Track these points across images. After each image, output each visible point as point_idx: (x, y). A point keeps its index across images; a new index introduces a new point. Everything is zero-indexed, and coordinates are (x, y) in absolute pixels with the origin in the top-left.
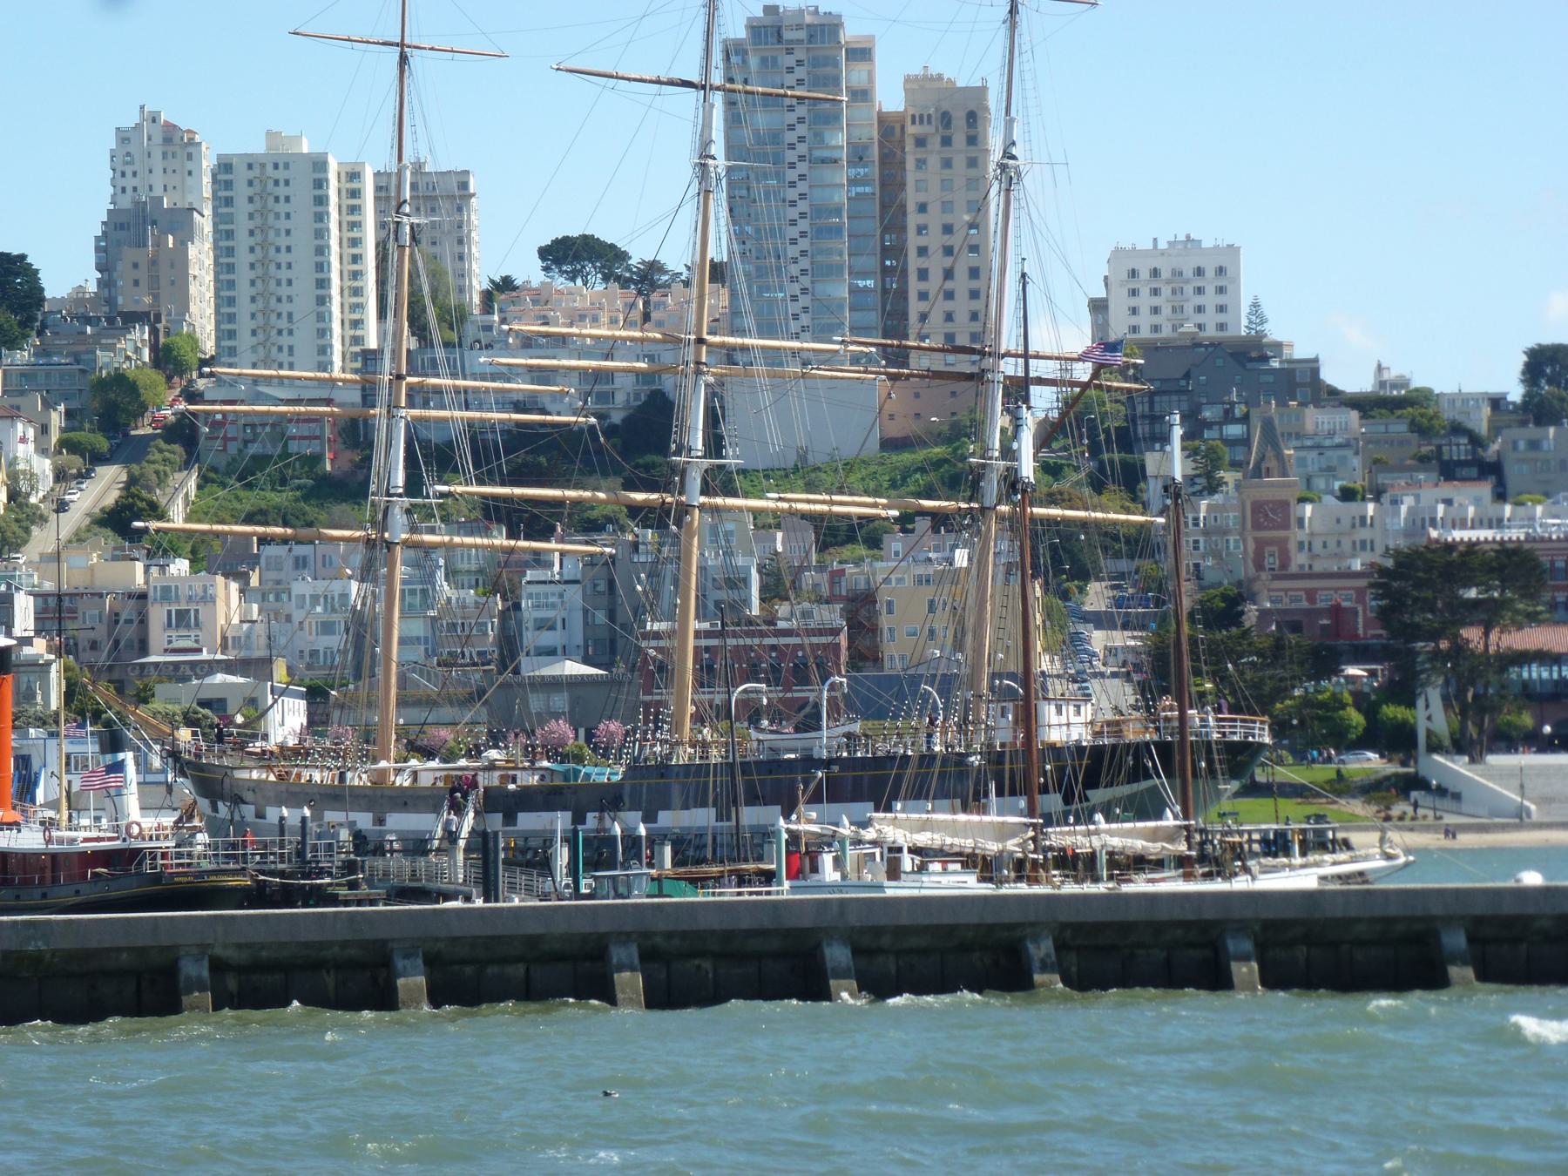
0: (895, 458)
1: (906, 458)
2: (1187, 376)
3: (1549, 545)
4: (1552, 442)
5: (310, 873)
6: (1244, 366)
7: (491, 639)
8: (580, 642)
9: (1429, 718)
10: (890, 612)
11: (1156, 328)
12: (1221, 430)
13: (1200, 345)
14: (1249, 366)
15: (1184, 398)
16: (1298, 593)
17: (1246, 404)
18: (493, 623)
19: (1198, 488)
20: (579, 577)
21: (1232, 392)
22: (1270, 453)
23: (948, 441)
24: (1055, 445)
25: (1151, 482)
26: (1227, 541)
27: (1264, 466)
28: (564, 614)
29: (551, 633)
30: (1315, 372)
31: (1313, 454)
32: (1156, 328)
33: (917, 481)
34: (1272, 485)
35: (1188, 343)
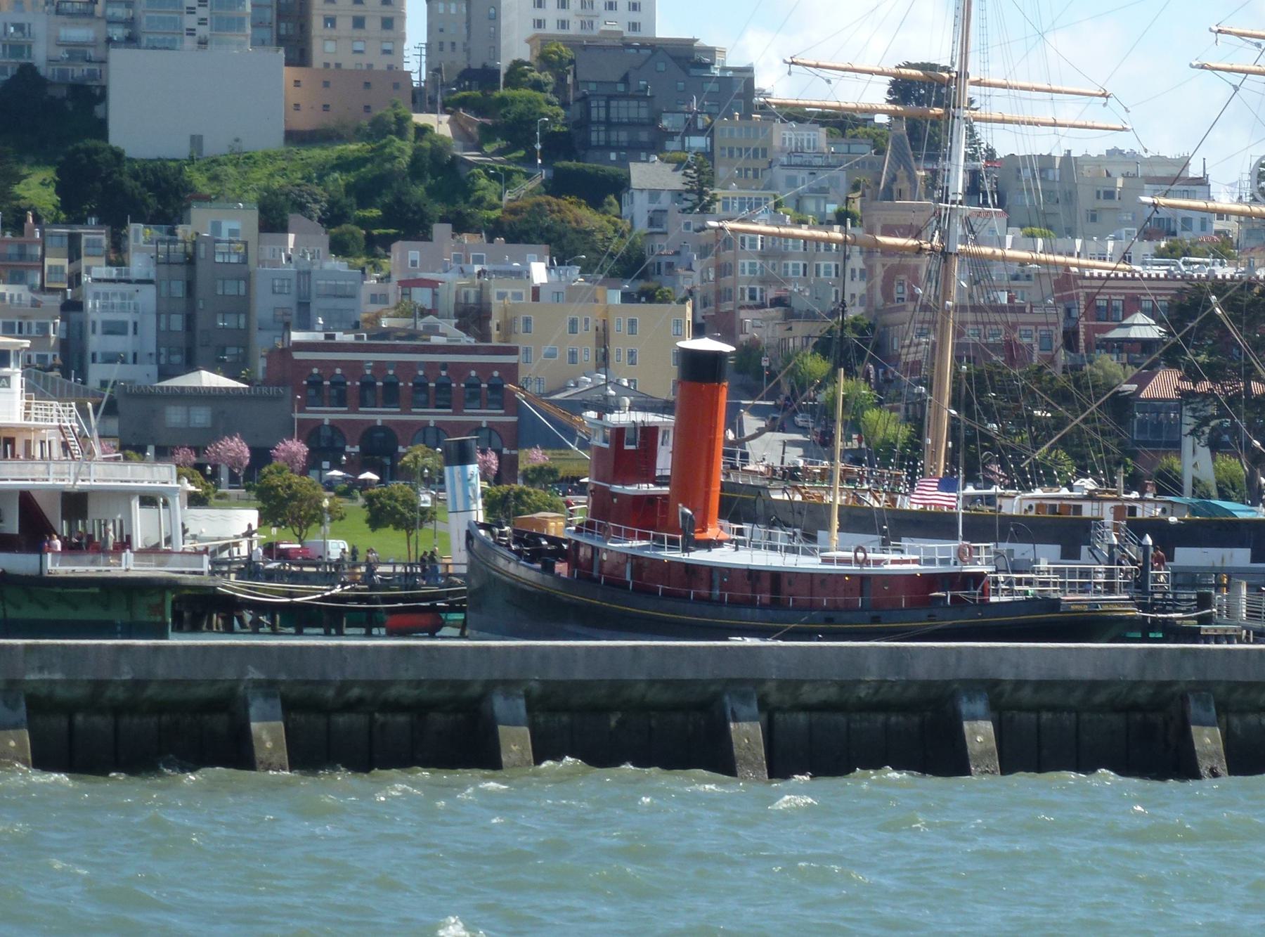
0: (304, 153)
1: (318, 154)
2: (625, 79)
3: (1133, 284)
4: (1057, 172)
5: (1153, 604)
6: (687, 72)
7: (52, 342)
8: (153, 350)
9: (1195, 465)
10: (527, 331)
11: (563, 24)
12: (683, 141)
13: (629, 46)
14: (694, 72)
15: (643, 104)
16: (1028, 327)
17: (710, 114)
18: (54, 324)
19: (689, 204)
20: (152, 276)
21: (692, 100)
22: (902, 173)
23: (368, 137)
24: (488, 148)
25: (637, 196)
26: (786, 266)
27: (895, 187)
28: (137, 318)
29: (122, 338)
30: (750, 81)
31: (802, 174)
32: (563, 24)
33: (336, 180)
34: (903, 207)
35: (618, 43)
